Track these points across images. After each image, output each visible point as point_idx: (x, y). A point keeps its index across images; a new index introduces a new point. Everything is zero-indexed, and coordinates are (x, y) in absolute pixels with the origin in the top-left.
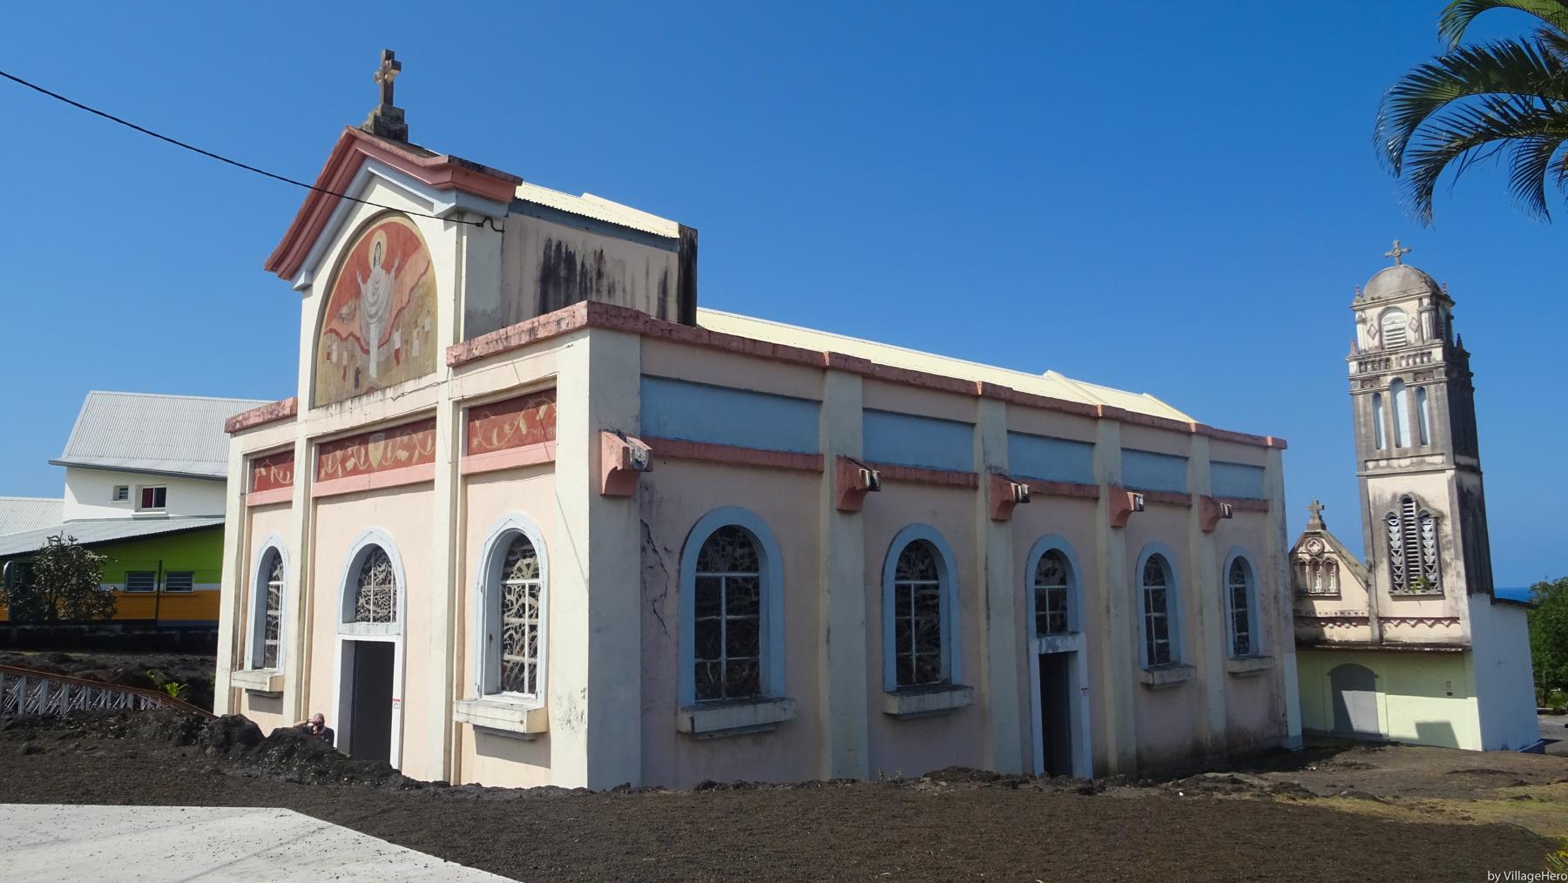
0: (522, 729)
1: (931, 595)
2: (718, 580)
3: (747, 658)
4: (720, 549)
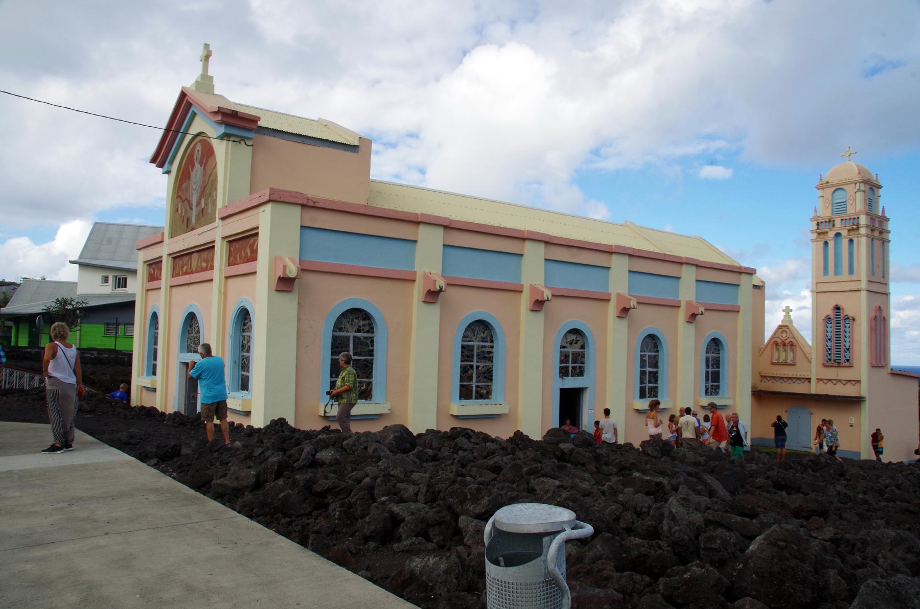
0: (240, 409)
1: (488, 352)
2: (348, 338)
3: (365, 380)
4: (350, 321)
